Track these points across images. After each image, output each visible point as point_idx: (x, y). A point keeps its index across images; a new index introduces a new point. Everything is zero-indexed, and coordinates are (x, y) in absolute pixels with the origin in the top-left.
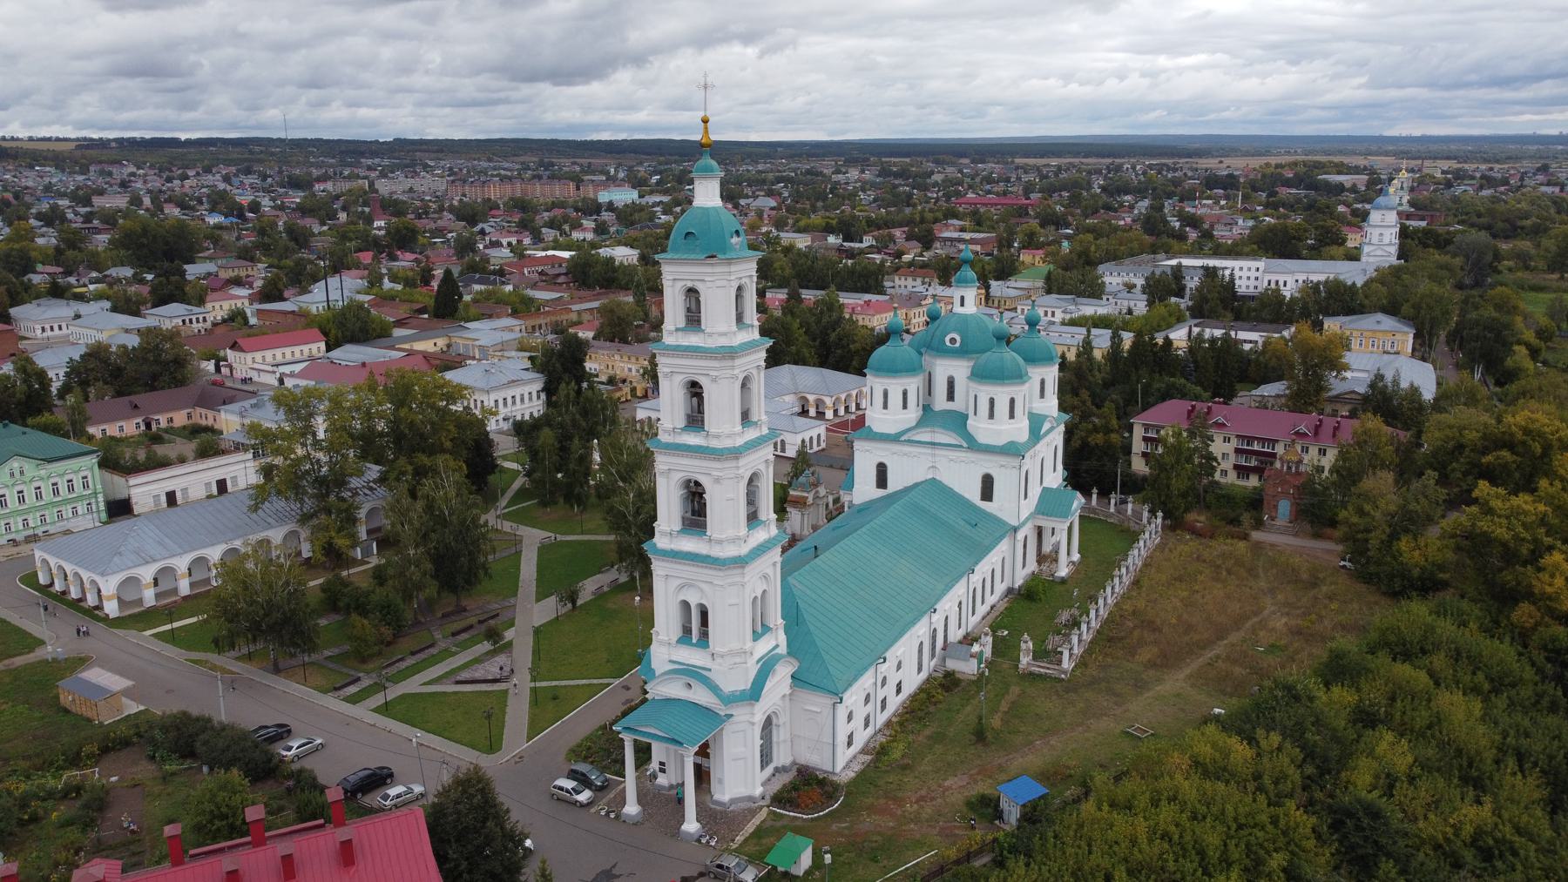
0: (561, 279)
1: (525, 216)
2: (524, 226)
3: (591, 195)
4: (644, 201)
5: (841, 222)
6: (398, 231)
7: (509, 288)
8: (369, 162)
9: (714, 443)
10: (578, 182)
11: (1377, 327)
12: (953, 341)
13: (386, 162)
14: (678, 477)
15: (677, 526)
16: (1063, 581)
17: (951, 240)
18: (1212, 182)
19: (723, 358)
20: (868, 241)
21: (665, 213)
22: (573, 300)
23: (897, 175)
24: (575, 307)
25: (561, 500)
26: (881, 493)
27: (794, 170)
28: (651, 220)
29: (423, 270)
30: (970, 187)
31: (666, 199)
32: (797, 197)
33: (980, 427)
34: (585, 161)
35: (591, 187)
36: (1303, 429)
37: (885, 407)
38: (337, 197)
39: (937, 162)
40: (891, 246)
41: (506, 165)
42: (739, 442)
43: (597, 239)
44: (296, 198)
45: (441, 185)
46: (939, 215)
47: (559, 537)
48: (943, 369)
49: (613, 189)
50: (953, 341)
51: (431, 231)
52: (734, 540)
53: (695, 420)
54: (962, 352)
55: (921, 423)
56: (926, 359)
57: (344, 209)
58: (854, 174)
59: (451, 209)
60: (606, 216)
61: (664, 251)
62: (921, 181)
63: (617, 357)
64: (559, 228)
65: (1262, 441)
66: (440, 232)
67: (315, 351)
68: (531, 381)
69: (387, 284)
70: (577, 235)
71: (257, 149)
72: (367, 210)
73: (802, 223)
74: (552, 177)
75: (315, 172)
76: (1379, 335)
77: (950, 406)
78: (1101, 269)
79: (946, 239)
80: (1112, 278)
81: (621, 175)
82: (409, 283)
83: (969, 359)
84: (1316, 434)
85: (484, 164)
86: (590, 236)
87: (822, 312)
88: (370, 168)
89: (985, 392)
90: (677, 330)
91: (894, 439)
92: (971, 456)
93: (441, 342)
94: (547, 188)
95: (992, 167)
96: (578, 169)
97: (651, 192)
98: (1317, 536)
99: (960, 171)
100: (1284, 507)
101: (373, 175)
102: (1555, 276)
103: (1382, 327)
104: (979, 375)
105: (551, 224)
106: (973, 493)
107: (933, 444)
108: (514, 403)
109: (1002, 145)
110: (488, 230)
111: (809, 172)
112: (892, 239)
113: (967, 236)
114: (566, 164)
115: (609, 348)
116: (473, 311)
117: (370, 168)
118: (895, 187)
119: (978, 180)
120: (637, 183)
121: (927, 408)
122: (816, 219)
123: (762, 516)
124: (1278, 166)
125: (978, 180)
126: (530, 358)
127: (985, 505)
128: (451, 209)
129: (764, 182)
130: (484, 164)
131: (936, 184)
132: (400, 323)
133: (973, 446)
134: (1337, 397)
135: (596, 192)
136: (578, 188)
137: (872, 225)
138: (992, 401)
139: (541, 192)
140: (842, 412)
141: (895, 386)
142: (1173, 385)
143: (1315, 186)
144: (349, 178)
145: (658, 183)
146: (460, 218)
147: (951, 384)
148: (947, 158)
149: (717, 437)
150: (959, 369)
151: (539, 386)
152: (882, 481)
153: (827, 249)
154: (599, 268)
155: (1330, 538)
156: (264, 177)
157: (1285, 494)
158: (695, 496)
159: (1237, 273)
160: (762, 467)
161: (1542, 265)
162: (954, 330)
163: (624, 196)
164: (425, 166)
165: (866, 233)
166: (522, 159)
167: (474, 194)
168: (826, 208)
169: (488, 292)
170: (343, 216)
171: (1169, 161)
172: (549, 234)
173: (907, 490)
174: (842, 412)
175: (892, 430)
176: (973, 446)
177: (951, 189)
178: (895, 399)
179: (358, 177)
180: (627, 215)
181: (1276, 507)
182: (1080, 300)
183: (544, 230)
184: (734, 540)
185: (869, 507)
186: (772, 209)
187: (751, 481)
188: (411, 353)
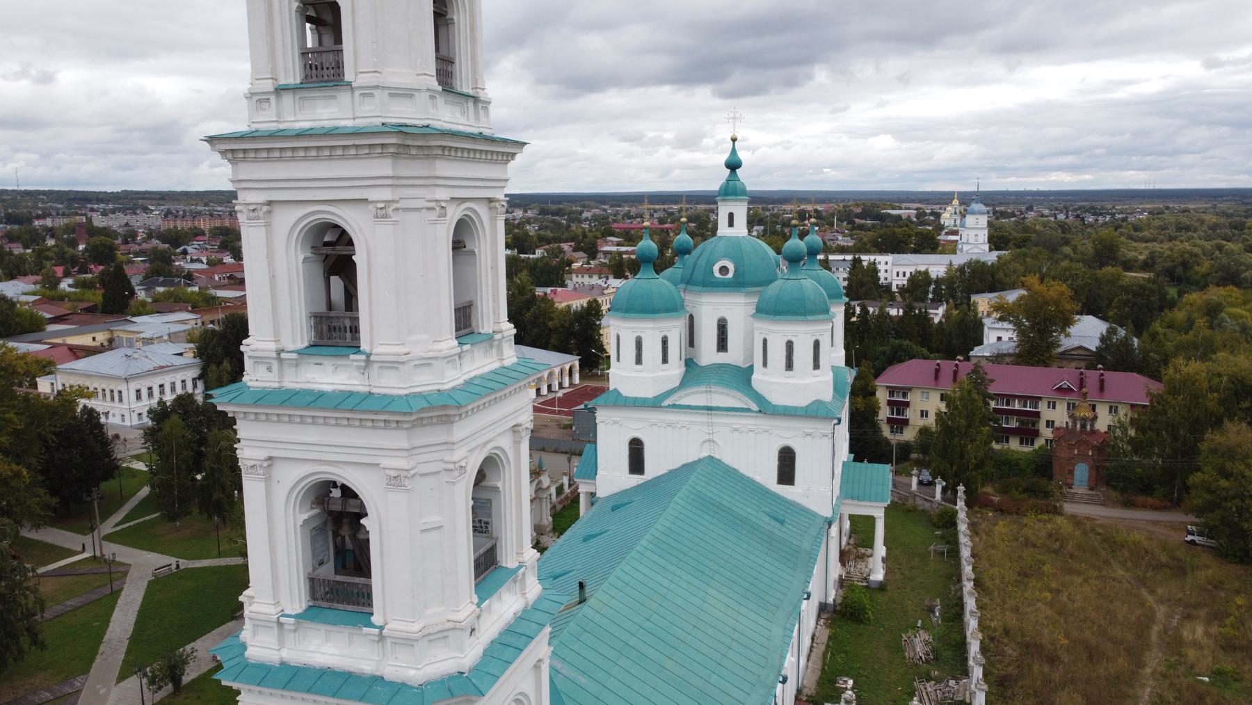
9: (388, 384)
12: (724, 270)
14: (292, 477)
15: (296, 599)
16: (882, 587)
19: (419, 423)
25: (196, 511)
26: (636, 480)
33: (772, 382)
36: (1065, 383)
37: (639, 360)
39: (584, 206)
42: (452, 378)
46: (598, 234)
47: (185, 564)
50: (724, 270)
52: (442, 635)
53: (336, 329)
54: (739, 284)
55: (686, 382)
56: (689, 298)
62: (575, 218)
77: (722, 358)
83: (748, 294)
89: (778, 333)
90: (280, 90)
91: (654, 404)
92: (764, 423)
98: (1128, 504)
100: (1082, 472)
104: (770, 310)
106: (767, 474)
112: (561, 251)
119: (619, 217)
121: (690, 363)
123: (508, 559)
125: (619, 217)
127: (785, 491)
131: (587, 219)
132: (58, 319)
133: (766, 409)
134: (1063, 353)
137: (543, 240)
138: (790, 346)
140: (544, 391)
141: (651, 331)
142: (900, 346)
143: (882, 218)
147: (722, 328)
148: (593, 204)
149: (393, 365)
150: (735, 309)
151: (195, 373)
152: (636, 462)
155: (1144, 506)
157: (1083, 457)
158: (340, 527)
160: (506, 443)
162: (725, 257)
165: (537, 247)
173: (672, 474)
174: (544, 391)
175: (650, 393)
176: (766, 409)
178: (652, 350)
181: (1071, 472)
184: (442, 635)
185: (620, 502)
187: (481, 476)
188: (54, 346)
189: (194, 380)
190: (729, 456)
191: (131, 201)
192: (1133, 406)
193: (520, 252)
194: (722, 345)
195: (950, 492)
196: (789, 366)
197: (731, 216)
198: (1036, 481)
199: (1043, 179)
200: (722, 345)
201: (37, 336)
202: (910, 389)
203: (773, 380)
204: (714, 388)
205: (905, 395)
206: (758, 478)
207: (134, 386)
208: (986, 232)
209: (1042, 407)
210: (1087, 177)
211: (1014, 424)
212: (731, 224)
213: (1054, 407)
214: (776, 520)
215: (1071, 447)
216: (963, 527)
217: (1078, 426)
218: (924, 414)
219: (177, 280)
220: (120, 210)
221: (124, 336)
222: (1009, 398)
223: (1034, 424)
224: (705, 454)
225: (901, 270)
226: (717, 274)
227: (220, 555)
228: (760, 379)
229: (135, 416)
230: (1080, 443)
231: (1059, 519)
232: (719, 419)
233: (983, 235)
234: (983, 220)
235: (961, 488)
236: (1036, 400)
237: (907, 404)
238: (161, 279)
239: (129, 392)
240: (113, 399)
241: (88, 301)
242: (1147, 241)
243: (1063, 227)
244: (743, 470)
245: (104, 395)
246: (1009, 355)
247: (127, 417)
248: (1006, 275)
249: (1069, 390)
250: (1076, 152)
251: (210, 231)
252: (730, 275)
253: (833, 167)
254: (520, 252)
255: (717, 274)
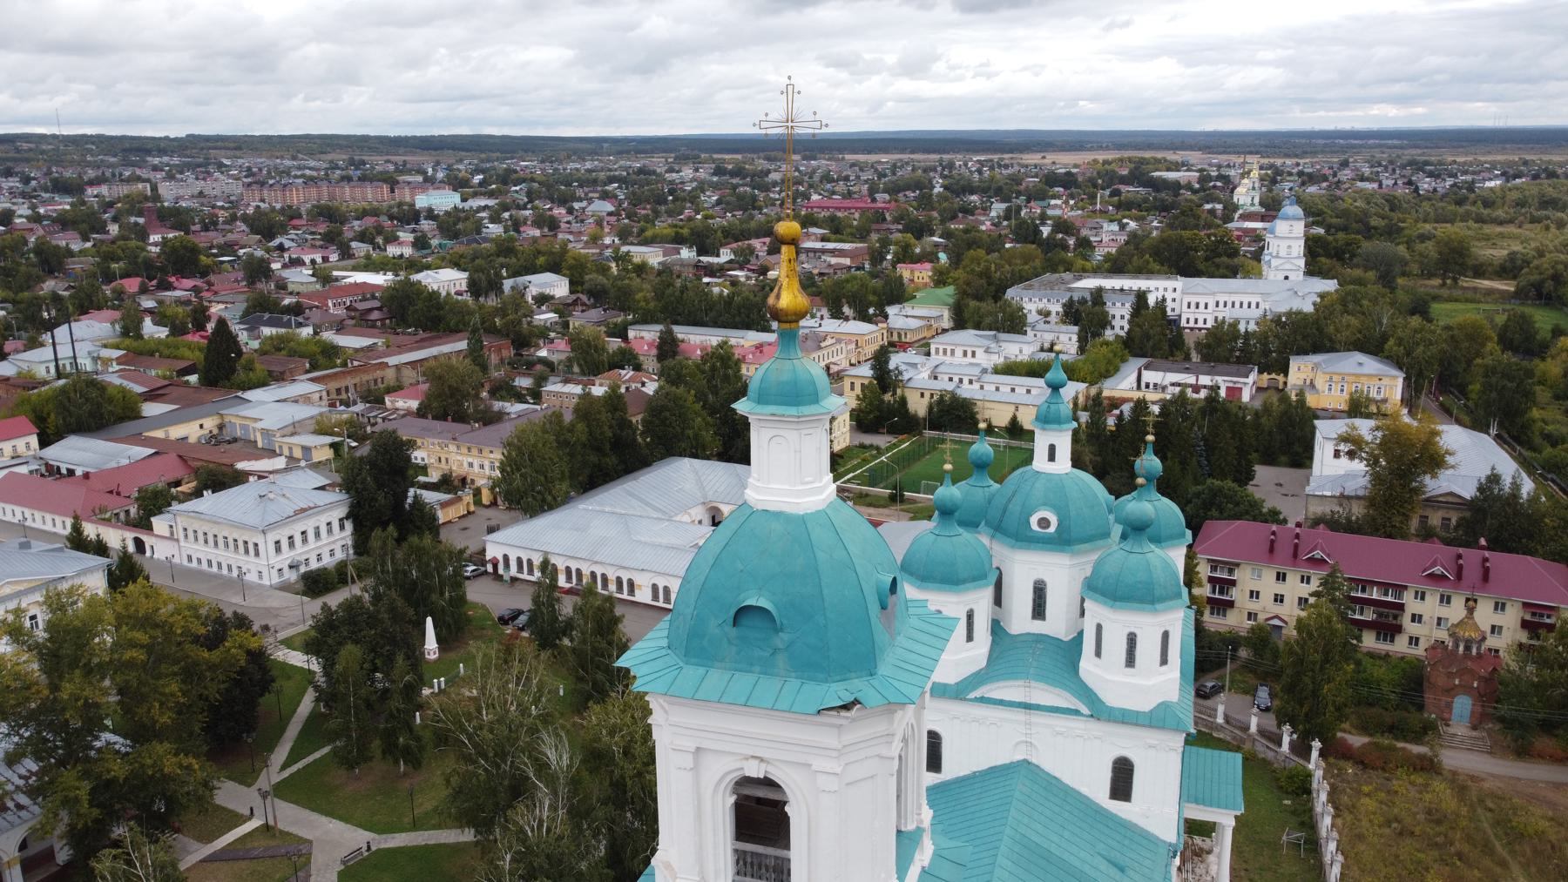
0: (375, 315)
1: (332, 226)
2: (331, 239)
3: (408, 199)
4: (467, 205)
5: (693, 232)
6: (174, 250)
7: (306, 332)
8: (156, 161)
10: (393, 184)
11: (1359, 370)
12: (1044, 523)
13: (176, 160)
17: (815, 251)
18: (1052, 180)
20: (725, 256)
21: (493, 220)
22: (391, 349)
23: (733, 174)
24: (393, 360)
27: (626, 169)
28: (479, 232)
29: (195, 311)
30: (811, 186)
31: (491, 202)
32: (636, 200)
34: (399, 159)
35: (407, 191)
38: (111, 205)
40: (753, 260)
41: (312, 163)
43: (417, 254)
44: (64, 204)
45: (236, 189)
48: (1023, 568)
49: (431, 192)
50: (1044, 523)
51: (219, 247)
54: (1063, 541)
57: (115, 219)
58: (687, 172)
59: (245, 219)
60: (426, 225)
61: (623, 648)
63: (452, 448)
64: (372, 242)
65: (1385, 587)
66: (229, 248)
67: (21, 448)
68: (331, 506)
69: (149, 328)
70: (393, 250)
71: (25, 146)
72: (141, 220)
73: (649, 233)
74: (363, 179)
75: (91, 173)
76: (1363, 380)
77: (1038, 627)
78: (1011, 293)
79: (808, 250)
80: (1032, 301)
81: (440, 175)
82: (177, 330)
84: (1459, 577)
85: (288, 163)
86: (408, 251)
87: (713, 369)
88: (155, 168)
92: (1095, 727)
93: (210, 423)
94: (358, 192)
95: (822, 164)
96: (391, 168)
97: (475, 195)
98: (1523, 752)
99: (797, 170)
100: (1463, 705)
101: (159, 175)
102: (1437, 282)
103: (1366, 370)
105: (362, 237)
106: (1097, 787)
107: (1027, 706)
108: (305, 541)
109: (829, 140)
110: (287, 244)
111: (641, 171)
112: (752, 250)
113: (830, 246)
114: (380, 163)
115: (440, 434)
116: (260, 368)
117: (155, 168)
118: (735, 187)
120: (457, 183)
122: (662, 226)
124: (1105, 162)
126: (332, 445)
127: (1117, 807)
128: (245, 219)
129: (595, 182)
130: (288, 163)
131: (775, 184)
132: (153, 395)
133: (1099, 711)
134: (1428, 500)
135: (412, 196)
136: (393, 191)
137: (730, 235)
139: (354, 196)
142: (1220, 490)
143: (1159, 185)
144: (129, 180)
145: (481, 184)
146: (254, 231)
150: (1063, 574)
151: (342, 512)
153: (683, 265)
154: (420, 305)
155: (1541, 756)
156: (26, 180)
157: (1466, 689)
159: (1169, 296)
161: (1415, 268)
162: (1046, 504)
163: (444, 200)
164: (220, 166)
165: (722, 245)
166: (329, 157)
167: (273, 201)
168: (670, 213)
169: (280, 338)
170: (114, 229)
171: (996, 157)
172: (360, 248)
176: (1099, 711)
177: (798, 190)
179: (140, 179)
180: (451, 224)
181: (1449, 706)
182: (1002, 336)
183: (354, 244)
186: (610, 214)
189: (341, 520)
190: (1050, 762)
191: (199, 153)
192: (1525, 605)
193: (699, 254)
194: (1039, 611)
195: (1302, 749)
196: (1130, 661)
197: (1052, 449)
198: (1405, 702)
199: (1359, 113)
200: (1039, 611)
201: (130, 427)
202: (1238, 565)
203: (1109, 677)
204: (1033, 684)
205: (1231, 571)
206: (1084, 790)
207: (272, 537)
208: (1302, 243)
209: (1408, 598)
210: (1420, 110)
211: (1369, 615)
212: (1052, 458)
213: (1423, 598)
214: (1115, 865)
215: (1450, 675)
216: (1321, 798)
217: (1461, 649)
218: (1254, 595)
219: (286, 318)
220: (191, 167)
221: (238, 421)
222: (1365, 584)
223: (1395, 617)
224: (1018, 757)
225: (1194, 300)
226: (1035, 527)
227: (415, 826)
228: (1088, 666)
229: (274, 573)
230: (1462, 672)
231: (1438, 785)
232: (1038, 718)
233: (1298, 247)
234: (1299, 228)
235: (1317, 744)
236: (1400, 589)
237: (1233, 583)
238: (267, 316)
239: (267, 547)
240: (247, 551)
241: (182, 358)
242: (1501, 223)
243: (1393, 203)
244: (1067, 779)
245: (236, 547)
246: (1358, 498)
247: (265, 574)
248: (1337, 330)
249: (1442, 578)
250: (1412, 79)
251: (309, 212)
252: (1052, 529)
253: (1095, 98)
254: (699, 254)
255: (1035, 527)
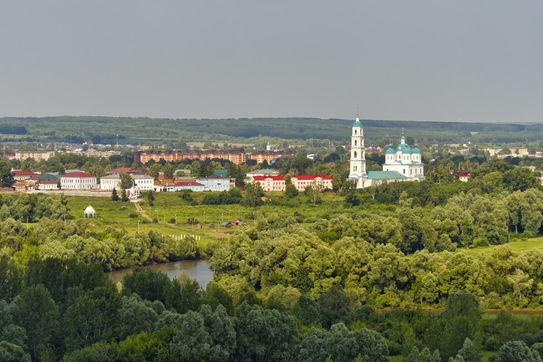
106: (402, 173)
176: (402, 165)
178: (390, 158)
